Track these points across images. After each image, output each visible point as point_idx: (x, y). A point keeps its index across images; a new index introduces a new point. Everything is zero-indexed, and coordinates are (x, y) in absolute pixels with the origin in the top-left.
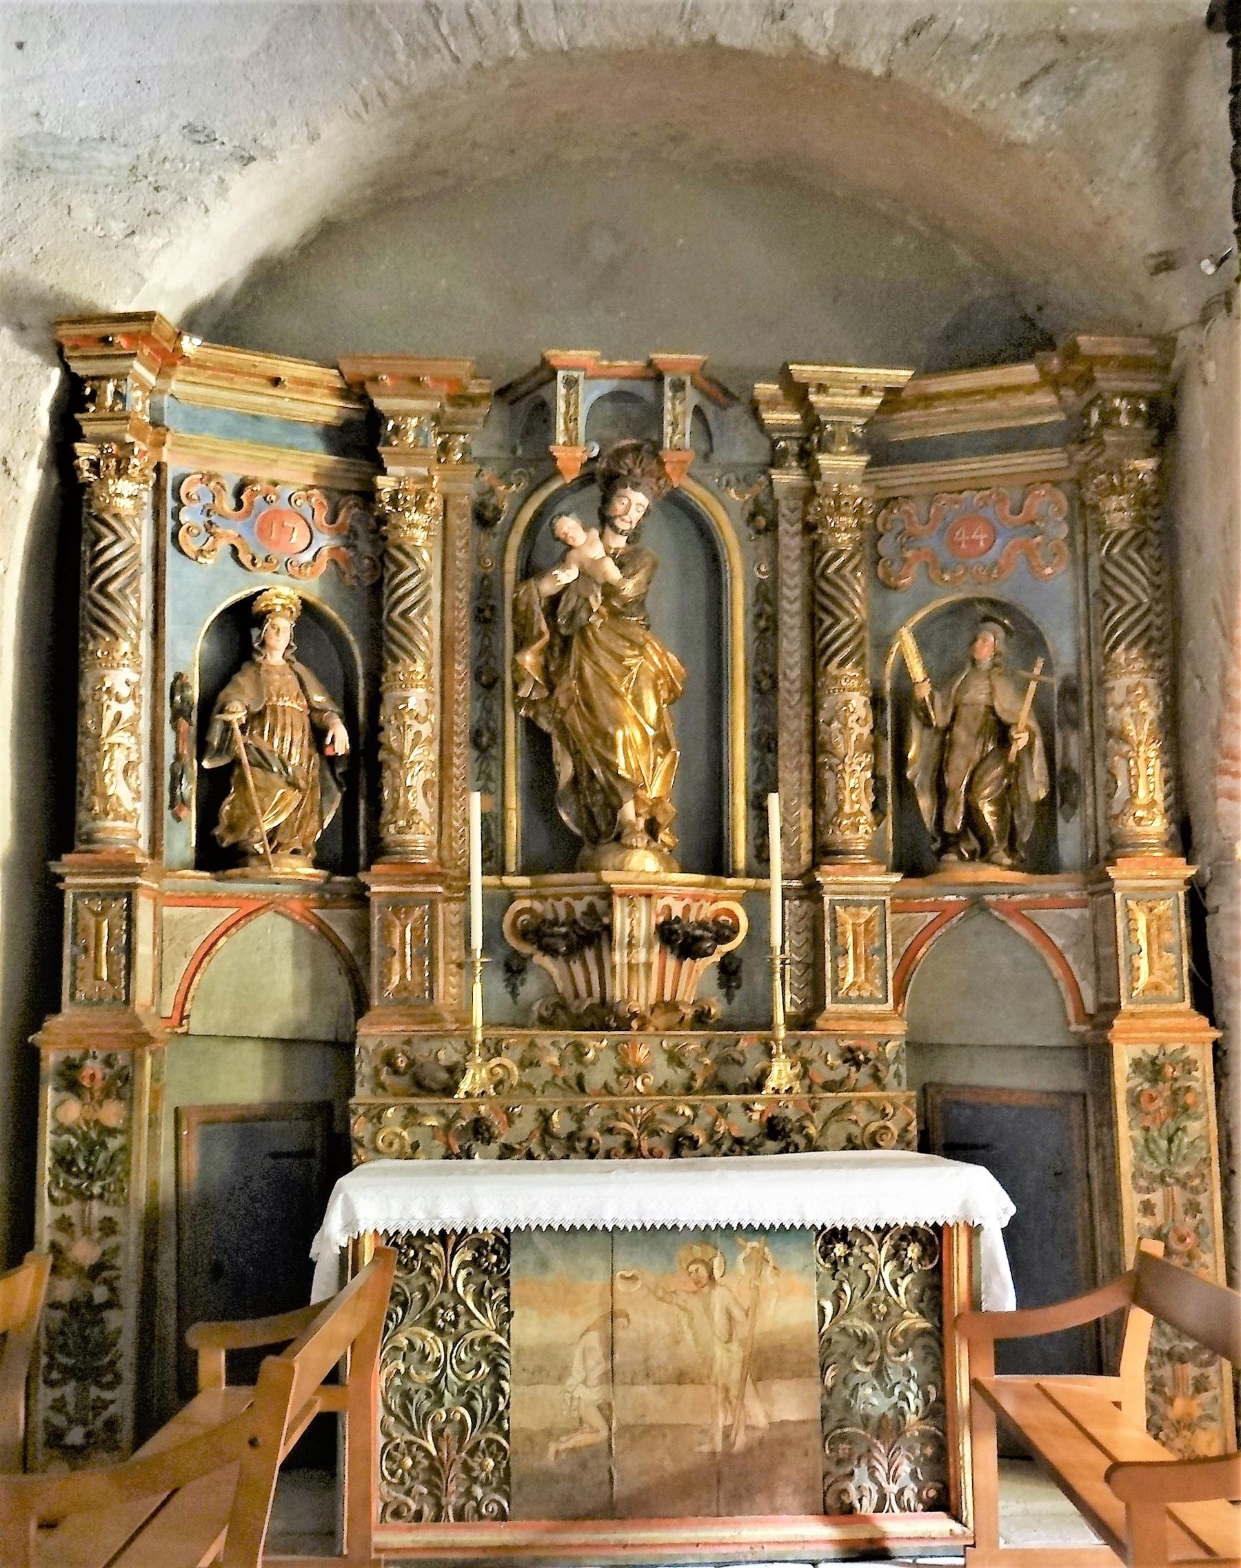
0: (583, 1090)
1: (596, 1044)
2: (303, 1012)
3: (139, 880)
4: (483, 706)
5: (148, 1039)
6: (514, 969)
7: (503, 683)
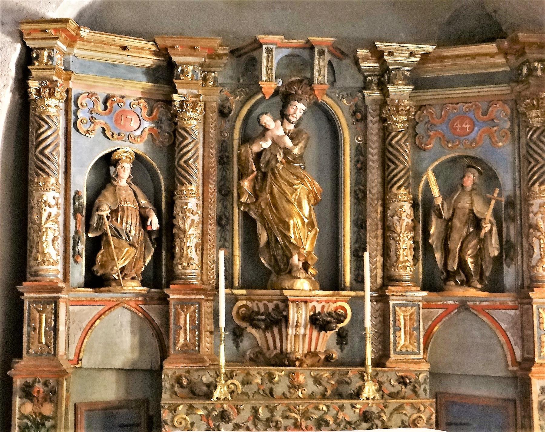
0: (272, 395)
1: (279, 373)
2: (136, 355)
3: (60, 295)
4: (223, 205)
5: (64, 373)
6: (237, 334)
7: (233, 194)
